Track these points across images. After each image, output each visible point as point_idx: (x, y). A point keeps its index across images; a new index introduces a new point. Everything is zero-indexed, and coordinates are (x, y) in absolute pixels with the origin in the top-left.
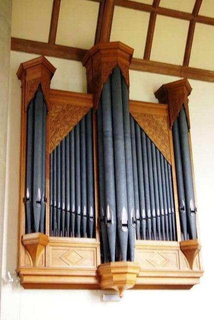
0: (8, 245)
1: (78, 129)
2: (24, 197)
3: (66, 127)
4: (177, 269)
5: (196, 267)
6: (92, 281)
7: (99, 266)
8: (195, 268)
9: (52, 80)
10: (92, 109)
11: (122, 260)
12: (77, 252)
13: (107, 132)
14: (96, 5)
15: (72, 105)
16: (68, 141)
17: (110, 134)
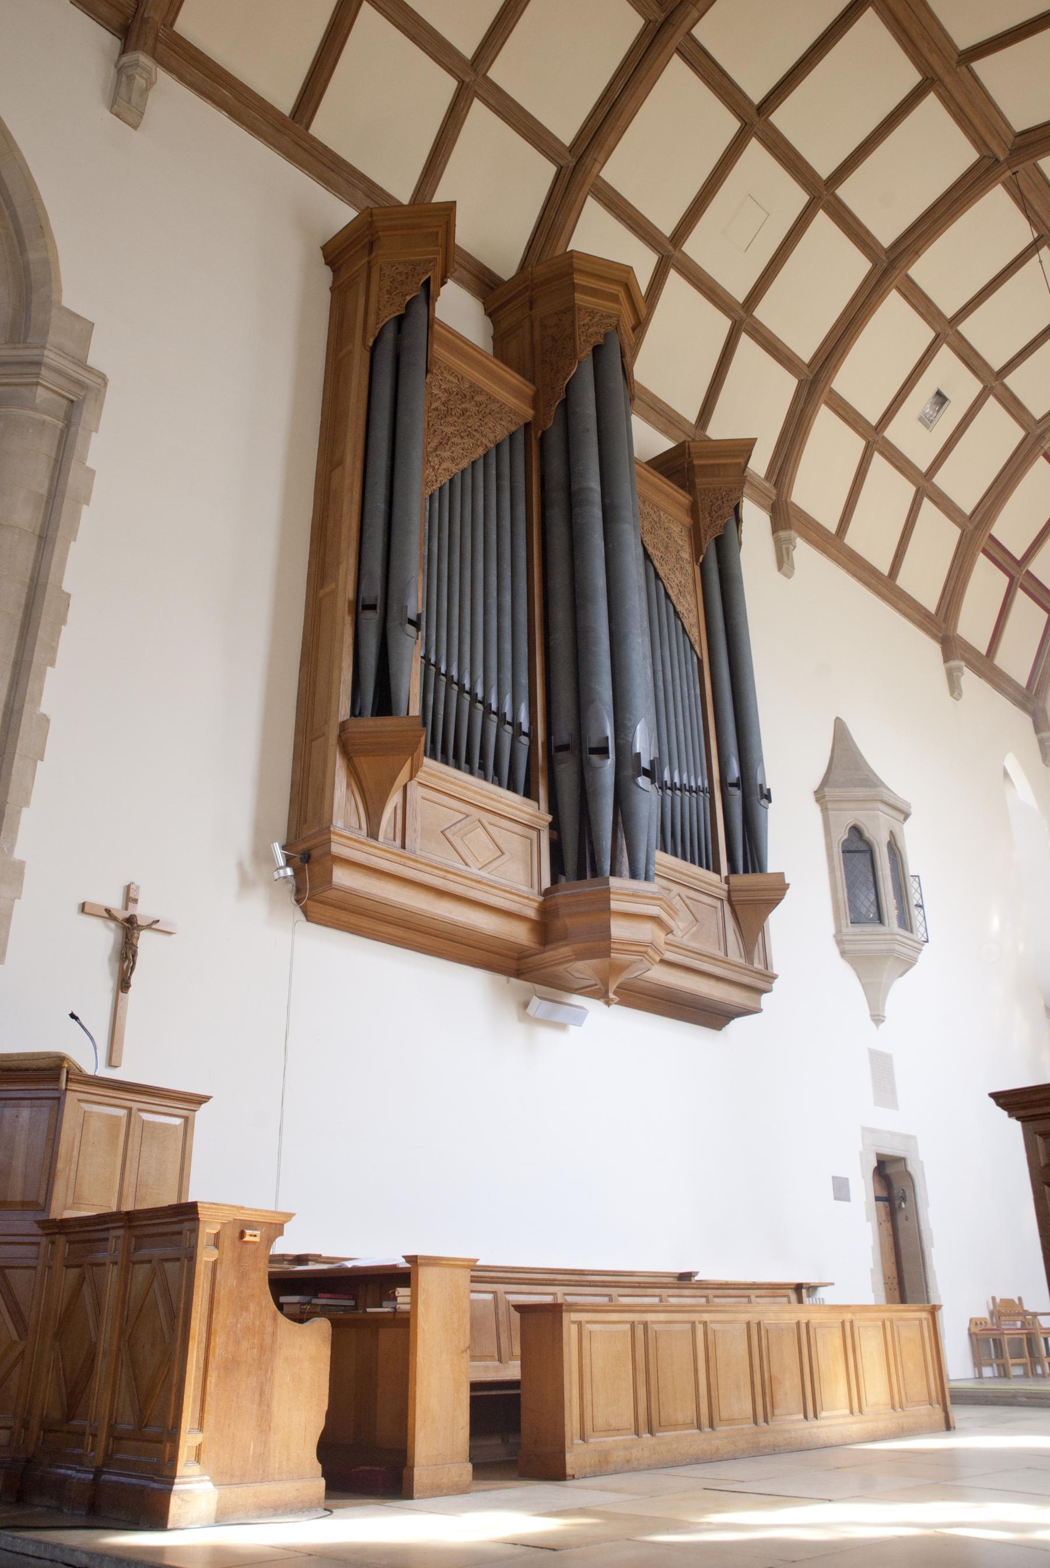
0: (612, 743)
1: (492, 461)
2: (350, 594)
3: (468, 442)
4: (721, 954)
5: (760, 963)
6: (520, 934)
7: (546, 893)
8: (758, 965)
9: (443, 287)
10: (527, 426)
11: (585, 878)
12: (490, 828)
13: (591, 489)
14: (632, 24)
15: (482, 391)
16: (492, 461)
17: (596, 497)
